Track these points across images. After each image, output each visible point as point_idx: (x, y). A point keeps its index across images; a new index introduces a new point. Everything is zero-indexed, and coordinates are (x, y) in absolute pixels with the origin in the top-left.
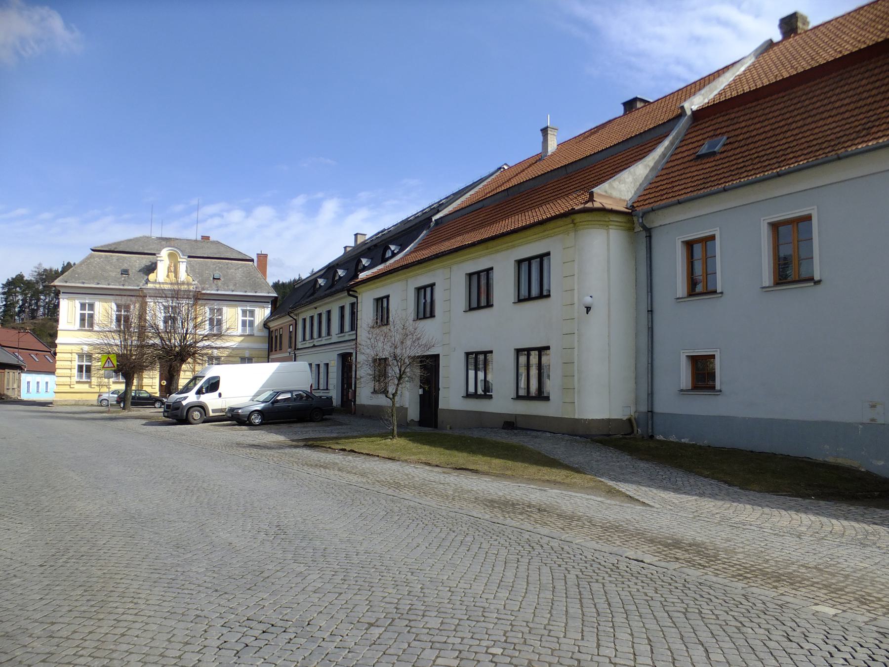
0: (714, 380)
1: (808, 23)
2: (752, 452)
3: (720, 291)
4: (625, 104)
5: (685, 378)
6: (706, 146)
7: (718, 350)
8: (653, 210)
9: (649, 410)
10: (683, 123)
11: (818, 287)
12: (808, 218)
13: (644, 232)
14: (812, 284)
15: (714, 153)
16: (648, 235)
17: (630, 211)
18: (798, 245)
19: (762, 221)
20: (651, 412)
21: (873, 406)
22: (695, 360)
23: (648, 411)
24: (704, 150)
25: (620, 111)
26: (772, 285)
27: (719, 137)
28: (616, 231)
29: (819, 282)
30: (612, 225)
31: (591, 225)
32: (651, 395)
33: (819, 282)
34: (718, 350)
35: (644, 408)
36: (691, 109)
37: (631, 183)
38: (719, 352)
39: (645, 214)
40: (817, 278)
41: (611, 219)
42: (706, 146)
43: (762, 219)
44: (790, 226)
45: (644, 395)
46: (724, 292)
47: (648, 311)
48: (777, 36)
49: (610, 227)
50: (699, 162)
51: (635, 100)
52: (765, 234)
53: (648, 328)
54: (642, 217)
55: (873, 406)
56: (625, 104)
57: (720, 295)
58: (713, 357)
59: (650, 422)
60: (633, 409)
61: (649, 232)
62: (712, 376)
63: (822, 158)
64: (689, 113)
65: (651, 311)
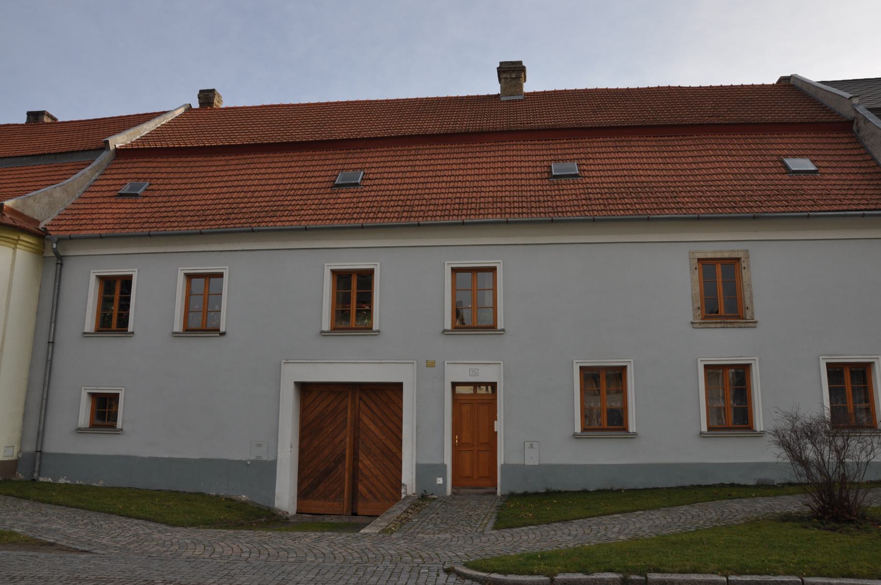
0: (116, 420)
1: (221, 104)
2: (147, 489)
3: (131, 331)
4: (30, 114)
5: (84, 417)
6: (128, 187)
7: (123, 389)
8: (70, 238)
9: (39, 450)
10: (105, 156)
11: (222, 338)
12: (220, 275)
13: (56, 258)
14: (218, 335)
15: (137, 195)
16: (59, 262)
17: (44, 234)
18: (208, 297)
19: (179, 270)
20: (40, 452)
21: (259, 445)
22: (835, 371)
23: (36, 451)
24: (125, 190)
25: (22, 120)
26: (181, 331)
27: (141, 182)
28: (24, 251)
29: (223, 334)
30: (21, 245)
31: (6, 241)
32: (41, 434)
33: (223, 334)
34: (123, 389)
35: (30, 448)
36: (115, 146)
37: (46, 204)
38: (123, 390)
39: (60, 240)
40: (222, 329)
41: (21, 238)
42: (128, 187)
43: (180, 269)
44: (203, 280)
45: (32, 434)
46: (135, 332)
47: (49, 342)
48: (196, 105)
49: (18, 246)
50: (120, 200)
51: (42, 113)
52: (181, 281)
53: (47, 360)
54: (56, 243)
55: (259, 445)
56: (30, 114)
57: (131, 335)
58: (116, 396)
59: (38, 463)
60: (16, 450)
61: (60, 260)
62: (114, 417)
63: (231, 227)
64: (112, 147)
65: (51, 343)
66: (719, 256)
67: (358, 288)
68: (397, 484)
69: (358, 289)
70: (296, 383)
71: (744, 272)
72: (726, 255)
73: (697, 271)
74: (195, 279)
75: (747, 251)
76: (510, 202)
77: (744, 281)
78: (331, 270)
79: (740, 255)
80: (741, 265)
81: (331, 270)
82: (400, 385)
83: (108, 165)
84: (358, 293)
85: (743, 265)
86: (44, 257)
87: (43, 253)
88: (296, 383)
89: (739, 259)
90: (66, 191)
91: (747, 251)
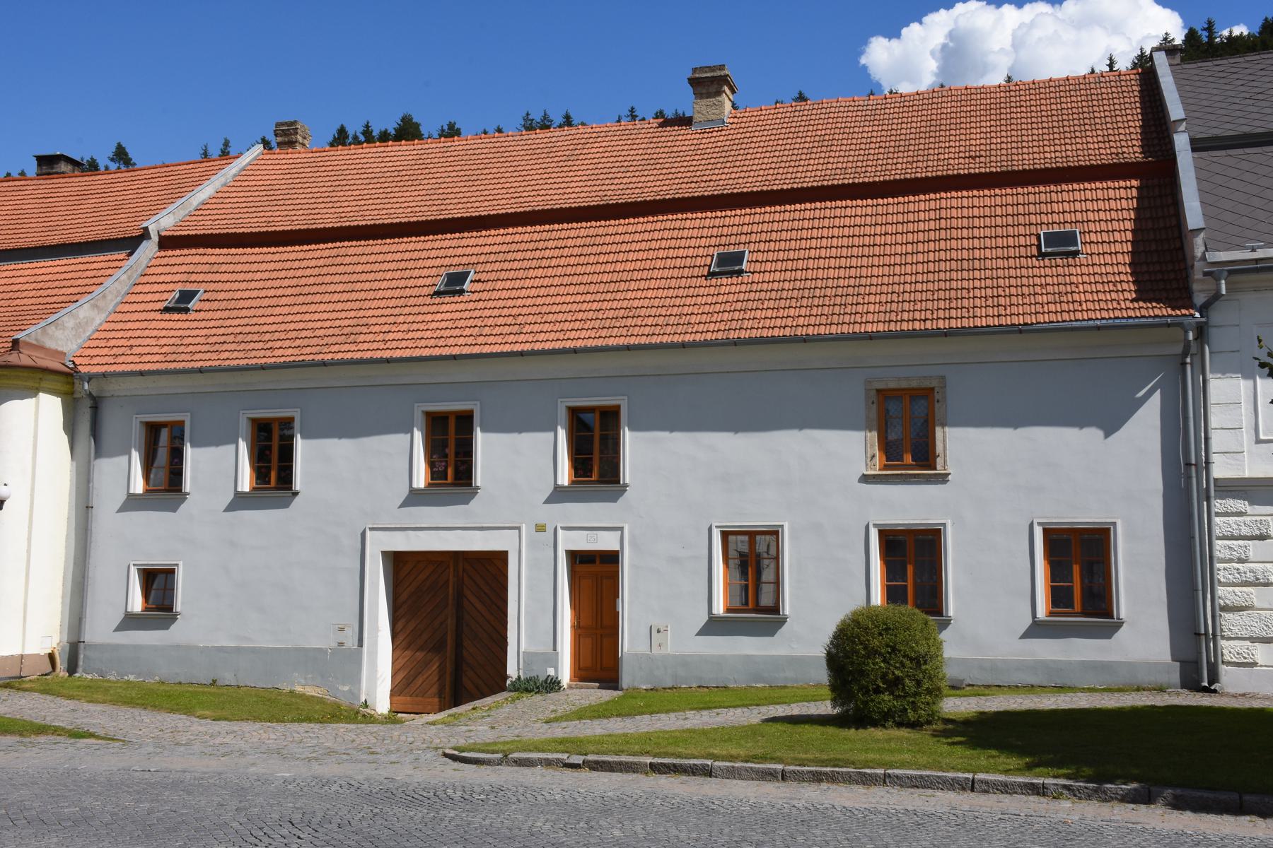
10: (148, 250)
21: (342, 630)
55: (342, 630)
66: (904, 385)
67: (457, 433)
68: (505, 677)
69: (456, 434)
70: (384, 553)
71: (937, 405)
72: (914, 384)
73: (875, 406)
74: (1178, 669)
75: (943, 378)
76: (968, 289)
77: (936, 418)
78: (423, 411)
79: (934, 384)
80: (934, 397)
81: (423, 411)
82: (506, 553)
83: (222, 186)
84: (456, 439)
85: (937, 396)
86: (74, 399)
87: (73, 393)
88: (384, 553)
89: (932, 389)
90: (97, 306)
91: (943, 378)
